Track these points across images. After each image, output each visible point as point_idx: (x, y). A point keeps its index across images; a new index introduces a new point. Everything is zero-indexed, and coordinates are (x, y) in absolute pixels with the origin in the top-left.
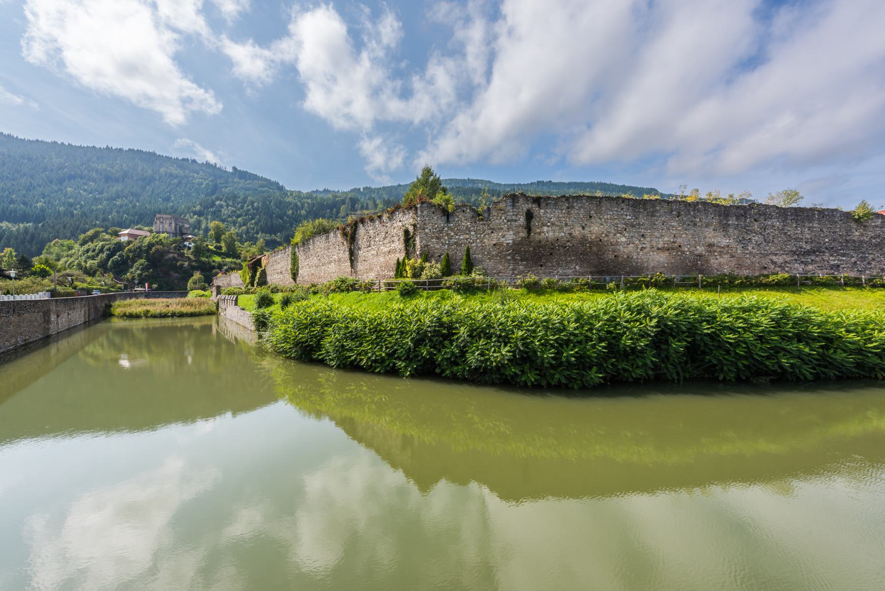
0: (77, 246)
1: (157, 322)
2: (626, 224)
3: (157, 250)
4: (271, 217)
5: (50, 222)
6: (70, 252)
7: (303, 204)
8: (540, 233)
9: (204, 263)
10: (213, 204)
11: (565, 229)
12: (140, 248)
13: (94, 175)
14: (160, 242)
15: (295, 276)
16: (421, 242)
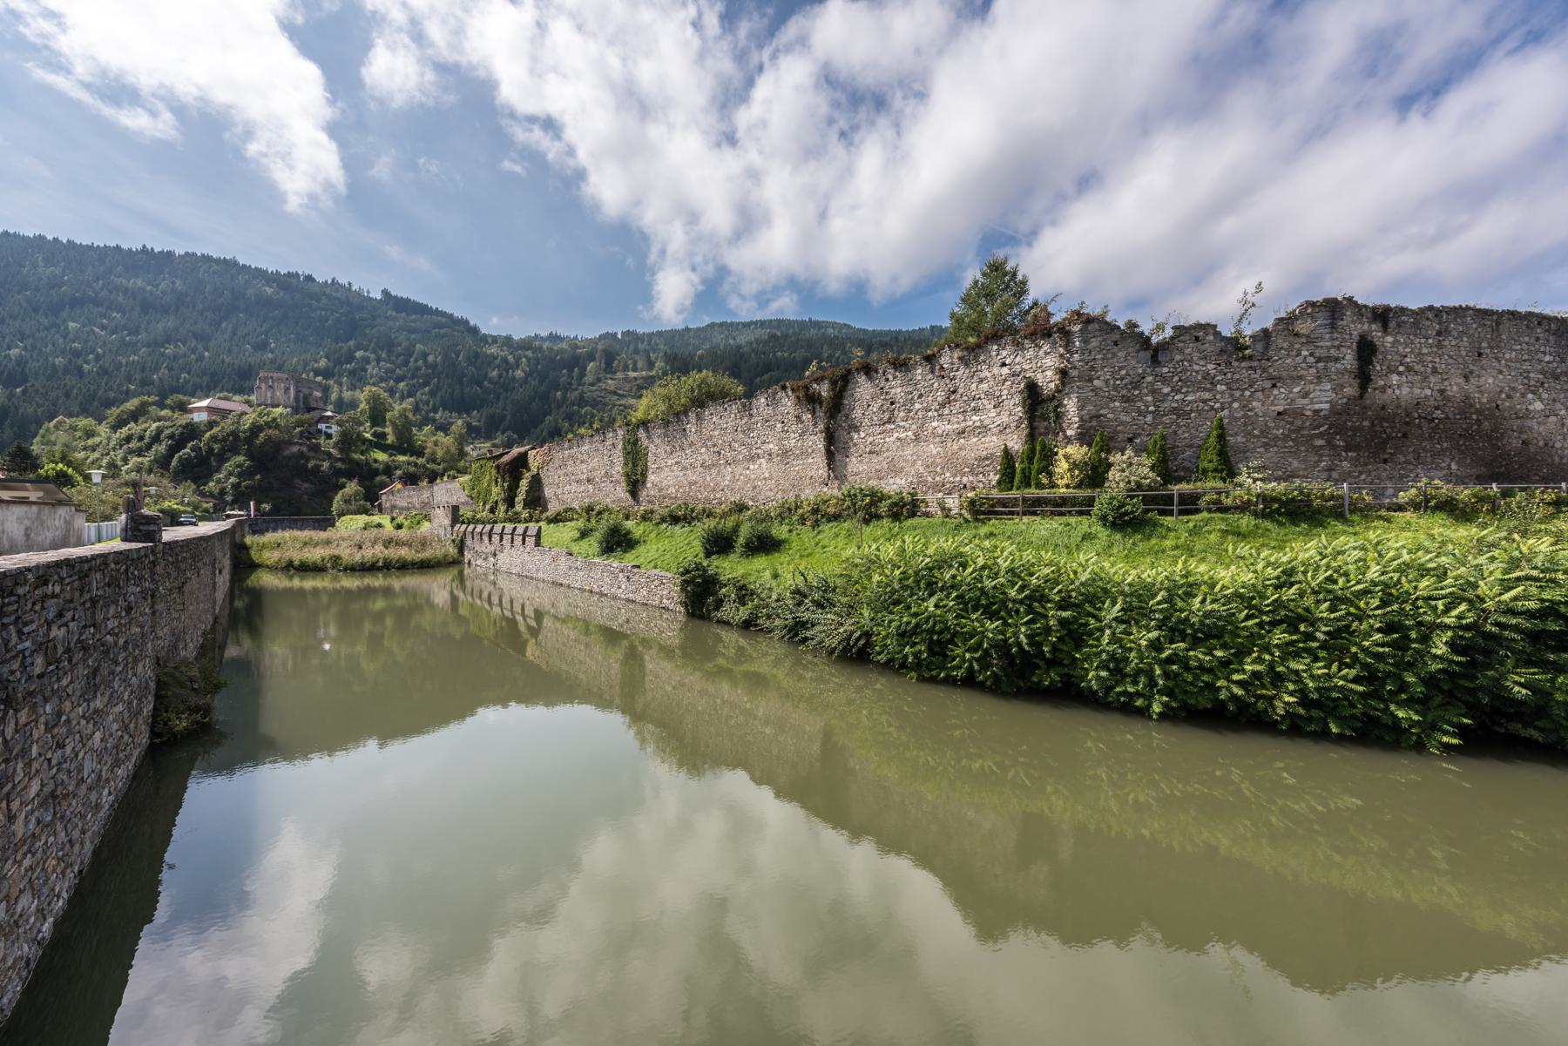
0: (103, 430)
1: (351, 583)
2: (1542, 372)
3: (269, 439)
4: (460, 381)
5: (37, 385)
6: (90, 442)
7: (518, 360)
8: (1383, 389)
9: (357, 463)
10: (350, 358)
11: (1432, 379)
12: (234, 434)
13: (120, 298)
14: (273, 424)
15: (635, 485)
16: (1081, 408)
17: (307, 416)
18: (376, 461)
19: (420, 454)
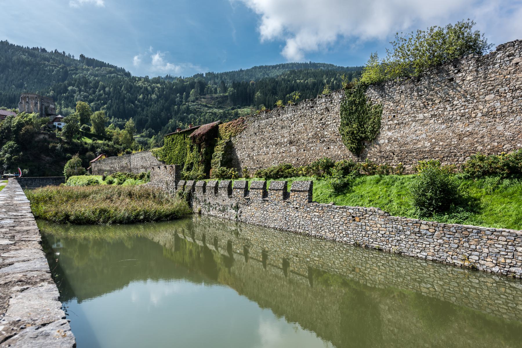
3: (27, 131)
4: (123, 101)
7: (153, 89)
9: (76, 145)
10: (65, 90)
12: (8, 128)
17: (47, 118)
18: (86, 143)
19: (110, 139)
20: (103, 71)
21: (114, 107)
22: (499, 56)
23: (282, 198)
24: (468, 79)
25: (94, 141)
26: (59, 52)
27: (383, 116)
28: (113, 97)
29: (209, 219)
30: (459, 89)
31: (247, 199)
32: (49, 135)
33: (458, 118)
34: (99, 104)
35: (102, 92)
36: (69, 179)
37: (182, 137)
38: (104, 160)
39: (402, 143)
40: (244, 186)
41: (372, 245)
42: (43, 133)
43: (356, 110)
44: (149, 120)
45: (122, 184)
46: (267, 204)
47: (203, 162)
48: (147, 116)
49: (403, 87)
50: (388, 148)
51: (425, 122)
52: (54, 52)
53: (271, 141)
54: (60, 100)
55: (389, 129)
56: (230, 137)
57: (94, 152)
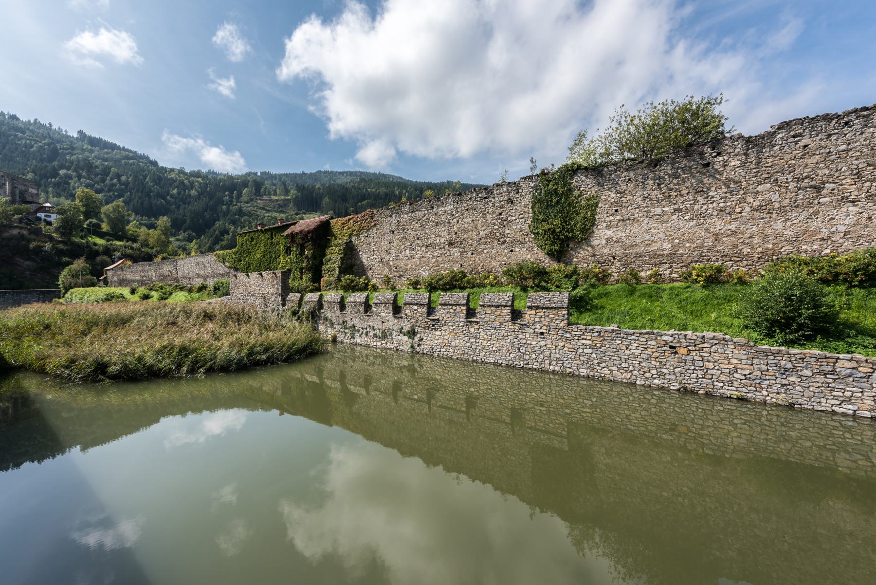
4: (148, 195)
9: (79, 246)
10: (55, 174)
17: (24, 206)
18: (95, 244)
19: (134, 240)
20: (116, 154)
21: (135, 201)
22: (780, 136)
23: (508, 317)
24: (733, 164)
25: (108, 241)
26: (42, 122)
27: (598, 210)
28: (133, 189)
29: (353, 350)
30: (718, 176)
31: (434, 320)
32: (29, 230)
33: (715, 213)
34: (111, 197)
35: (115, 181)
36: (69, 293)
37: (267, 236)
38: (130, 267)
39: (628, 244)
40: (427, 301)
41: (722, 391)
42: (17, 227)
43: (558, 202)
44: (188, 221)
45: (166, 298)
46: (477, 327)
47: (308, 269)
48: (184, 216)
49: (632, 174)
50: (605, 251)
51: (665, 218)
52: (32, 121)
53: (419, 242)
54: (45, 186)
55: (608, 227)
56: (351, 235)
57: (110, 256)
